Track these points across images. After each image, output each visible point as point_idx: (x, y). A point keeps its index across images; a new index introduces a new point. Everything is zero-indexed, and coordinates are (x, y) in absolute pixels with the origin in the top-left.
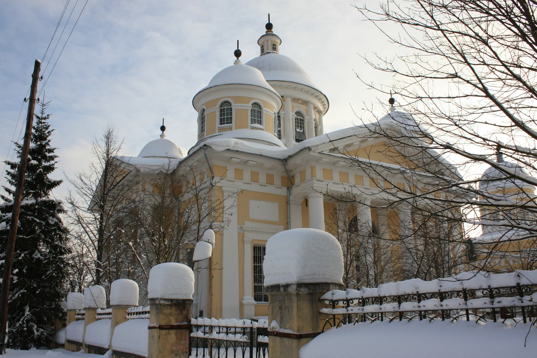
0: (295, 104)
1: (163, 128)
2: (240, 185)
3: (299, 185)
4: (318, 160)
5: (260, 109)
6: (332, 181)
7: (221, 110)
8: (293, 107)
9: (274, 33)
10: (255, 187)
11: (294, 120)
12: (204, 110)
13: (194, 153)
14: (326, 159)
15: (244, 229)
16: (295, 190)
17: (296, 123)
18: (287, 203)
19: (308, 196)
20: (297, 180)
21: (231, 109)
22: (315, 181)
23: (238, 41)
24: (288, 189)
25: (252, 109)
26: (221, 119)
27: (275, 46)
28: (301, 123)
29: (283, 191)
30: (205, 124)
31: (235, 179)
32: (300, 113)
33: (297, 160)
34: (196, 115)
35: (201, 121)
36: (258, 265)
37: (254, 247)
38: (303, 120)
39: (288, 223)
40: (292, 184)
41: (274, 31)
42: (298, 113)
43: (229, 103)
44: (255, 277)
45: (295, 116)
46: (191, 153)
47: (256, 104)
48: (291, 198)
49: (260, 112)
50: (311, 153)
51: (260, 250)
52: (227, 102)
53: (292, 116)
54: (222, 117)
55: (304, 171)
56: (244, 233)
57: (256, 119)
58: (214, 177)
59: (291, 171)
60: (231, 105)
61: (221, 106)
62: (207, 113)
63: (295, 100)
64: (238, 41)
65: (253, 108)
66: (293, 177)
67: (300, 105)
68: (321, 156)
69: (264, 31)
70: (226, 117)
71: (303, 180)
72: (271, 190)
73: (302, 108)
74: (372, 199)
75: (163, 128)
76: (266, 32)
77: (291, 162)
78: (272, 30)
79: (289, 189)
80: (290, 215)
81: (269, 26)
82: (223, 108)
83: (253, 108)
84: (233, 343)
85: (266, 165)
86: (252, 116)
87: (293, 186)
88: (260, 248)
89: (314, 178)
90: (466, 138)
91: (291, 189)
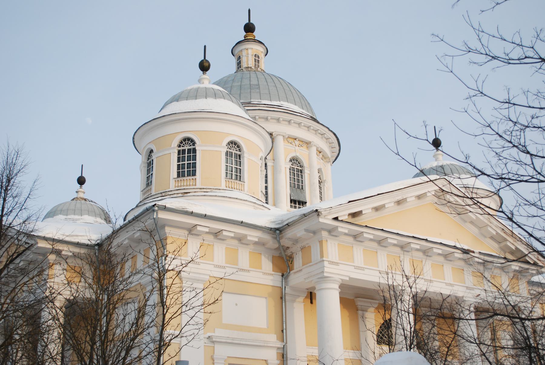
1: (81, 181)
3: (300, 270)
4: (331, 231)
6: (211, 263)
7: (179, 151)
11: (288, 171)
12: (152, 151)
13: (136, 219)
14: (343, 228)
15: (214, 339)
16: (296, 279)
18: (281, 298)
19: (314, 288)
20: (298, 262)
21: (194, 150)
22: (326, 264)
23: (205, 47)
24: (283, 276)
25: (227, 152)
26: (178, 165)
27: (258, 57)
31: (250, 267)
33: (298, 232)
35: (146, 169)
38: (301, 171)
39: (282, 331)
45: (289, 165)
46: (129, 218)
47: (233, 144)
48: (288, 290)
49: (240, 156)
50: (321, 220)
53: (285, 166)
54: (181, 163)
56: (214, 347)
59: (288, 248)
60: (194, 144)
61: (179, 146)
62: (157, 156)
64: (205, 47)
65: (229, 150)
68: (335, 223)
69: (241, 34)
71: (307, 261)
73: (301, 153)
74: (342, 280)
75: (81, 181)
77: (290, 233)
79: (285, 276)
80: (286, 317)
81: (249, 28)
82: (181, 148)
83: (229, 150)
85: (249, 238)
87: (291, 272)
89: (324, 259)
90: (21, 280)
91: (288, 276)
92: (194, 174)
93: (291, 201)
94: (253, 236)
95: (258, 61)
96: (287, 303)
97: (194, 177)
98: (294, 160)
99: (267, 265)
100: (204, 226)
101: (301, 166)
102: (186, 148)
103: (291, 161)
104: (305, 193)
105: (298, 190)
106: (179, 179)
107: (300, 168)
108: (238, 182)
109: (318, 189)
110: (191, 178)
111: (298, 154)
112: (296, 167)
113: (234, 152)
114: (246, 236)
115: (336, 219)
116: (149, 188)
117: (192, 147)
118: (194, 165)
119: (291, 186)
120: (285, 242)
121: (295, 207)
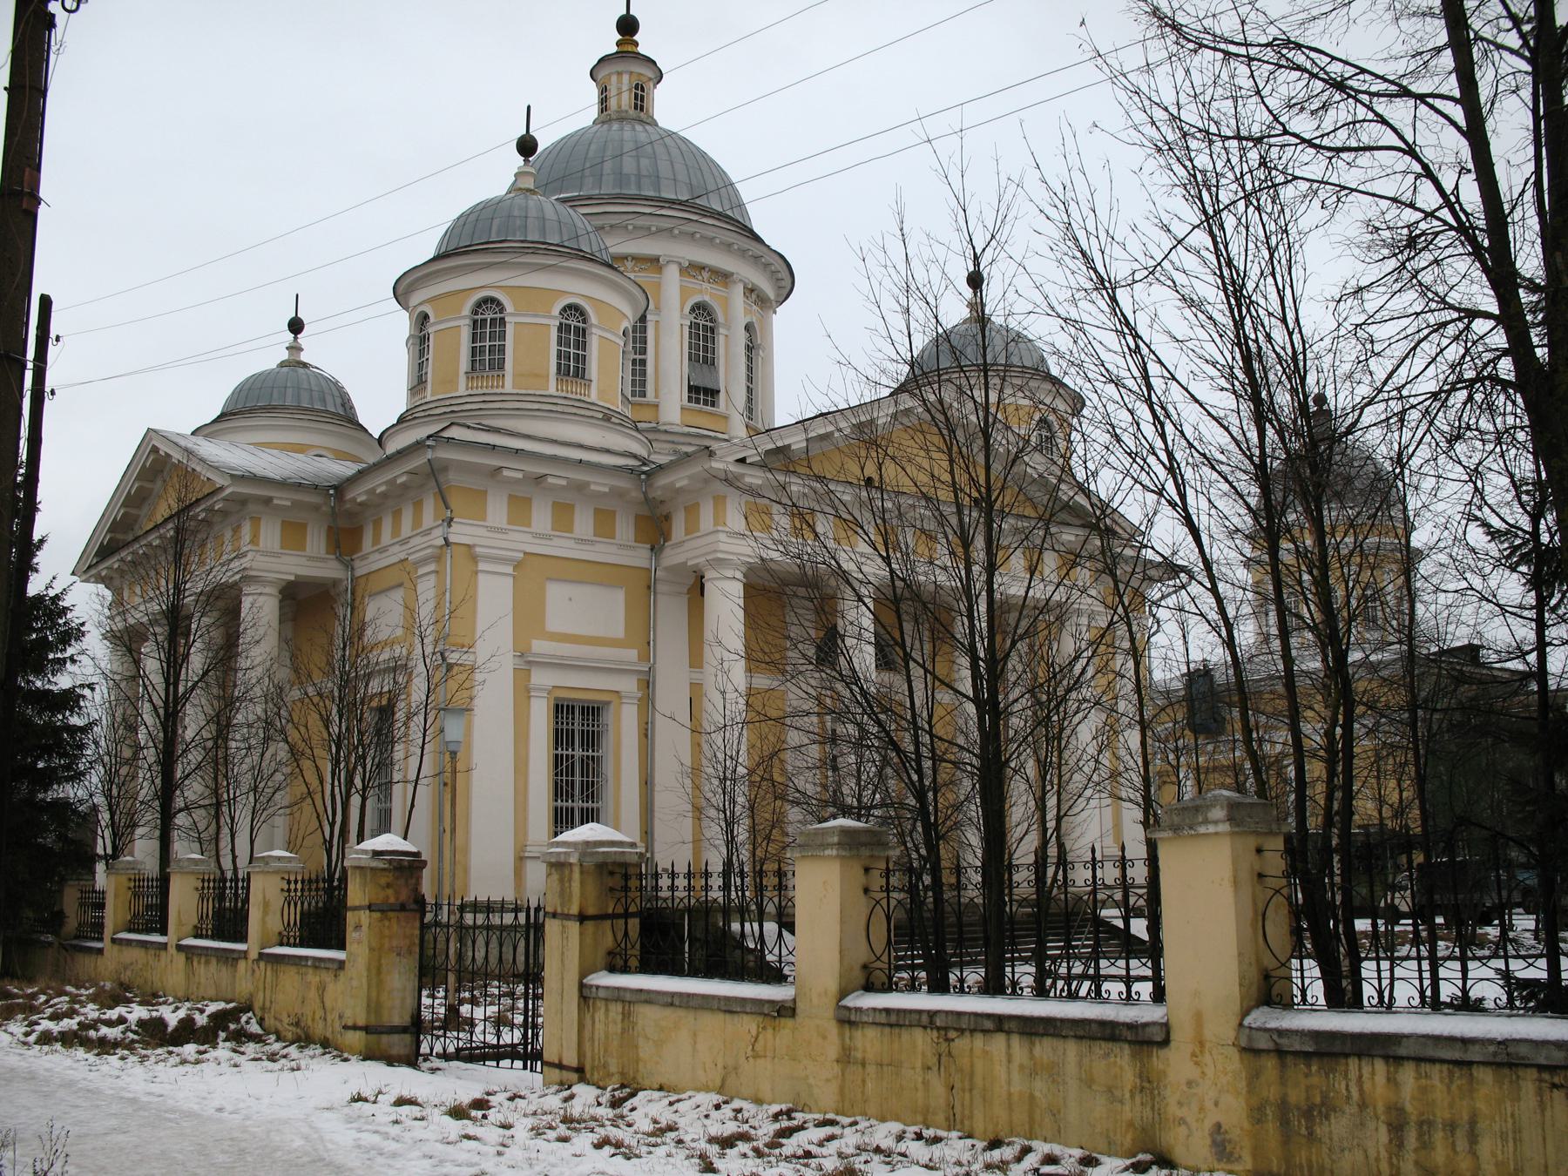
0: (691, 283)
1: (296, 326)
2: (520, 542)
5: (584, 321)
7: (475, 322)
8: (684, 293)
9: (641, 50)
10: (562, 547)
11: (686, 331)
17: (690, 338)
21: (503, 321)
23: (529, 108)
24: (652, 549)
25: (561, 324)
27: (643, 90)
28: (706, 339)
29: (639, 557)
30: (431, 356)
32: (704, 310)
34: (400, 323)
35: (418, 348)
36: (565, 752)
37: (557, 706)
40: (666, 536)
41: (646, 42)
42: (700, 309)
43: (499, 303)
44: (556, 783)
47: (572, 309)
49: (584, 330)
51: (573, 713)
52: (493, 300)
55: (697, 504)
57: (572, 351)
58: (451, 519)
61: (476, 313)
63: (694, 269)
64: (529, 108)
65: (564, 321)
66: (668, 518)
67: (706, 285)
69: (609, 42)
70: (488, 344)
71: (692, 528)
72: (604, 552)
75: (296, 326)
76: (618, 44)
78: (636, 38)
79: (656, 549)
81: (628, 26)
83: (564, 321)
84: (925, 1019)
85: (593, 487)
86: (559, 344)
88: (573, 707)
91: (662, 548)
92: (501, 367)
93: (691, 388)
94: (600, 484)
95: (642, 97)
96: (659, 596)
97: (501, 373)
98: (700, 309)
99: (625, 529)
100: (514, 471)
101: (711, 321)
102: (489, 316)
103: (693, 310)
104: (717, 372)
105: (705, 366)
106: (475, 375)
107: (709, 324)
108: (579, 381)
109: (743, 359)
110: (495, 374)
111: (707, 298)
112: (702, 323)
113: (573, 323)
114: (588, 484)
115: (742, 461)
116: (422, 386)
117: (498, 315)
118: (502, 349)
119: (690, 359)
120: (656, 493)
121: (698, 401)
